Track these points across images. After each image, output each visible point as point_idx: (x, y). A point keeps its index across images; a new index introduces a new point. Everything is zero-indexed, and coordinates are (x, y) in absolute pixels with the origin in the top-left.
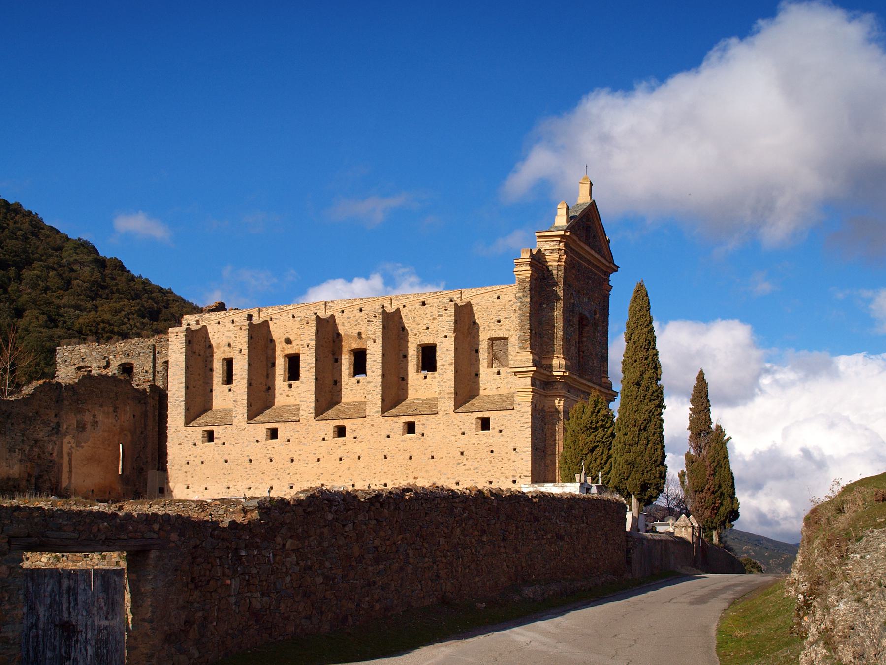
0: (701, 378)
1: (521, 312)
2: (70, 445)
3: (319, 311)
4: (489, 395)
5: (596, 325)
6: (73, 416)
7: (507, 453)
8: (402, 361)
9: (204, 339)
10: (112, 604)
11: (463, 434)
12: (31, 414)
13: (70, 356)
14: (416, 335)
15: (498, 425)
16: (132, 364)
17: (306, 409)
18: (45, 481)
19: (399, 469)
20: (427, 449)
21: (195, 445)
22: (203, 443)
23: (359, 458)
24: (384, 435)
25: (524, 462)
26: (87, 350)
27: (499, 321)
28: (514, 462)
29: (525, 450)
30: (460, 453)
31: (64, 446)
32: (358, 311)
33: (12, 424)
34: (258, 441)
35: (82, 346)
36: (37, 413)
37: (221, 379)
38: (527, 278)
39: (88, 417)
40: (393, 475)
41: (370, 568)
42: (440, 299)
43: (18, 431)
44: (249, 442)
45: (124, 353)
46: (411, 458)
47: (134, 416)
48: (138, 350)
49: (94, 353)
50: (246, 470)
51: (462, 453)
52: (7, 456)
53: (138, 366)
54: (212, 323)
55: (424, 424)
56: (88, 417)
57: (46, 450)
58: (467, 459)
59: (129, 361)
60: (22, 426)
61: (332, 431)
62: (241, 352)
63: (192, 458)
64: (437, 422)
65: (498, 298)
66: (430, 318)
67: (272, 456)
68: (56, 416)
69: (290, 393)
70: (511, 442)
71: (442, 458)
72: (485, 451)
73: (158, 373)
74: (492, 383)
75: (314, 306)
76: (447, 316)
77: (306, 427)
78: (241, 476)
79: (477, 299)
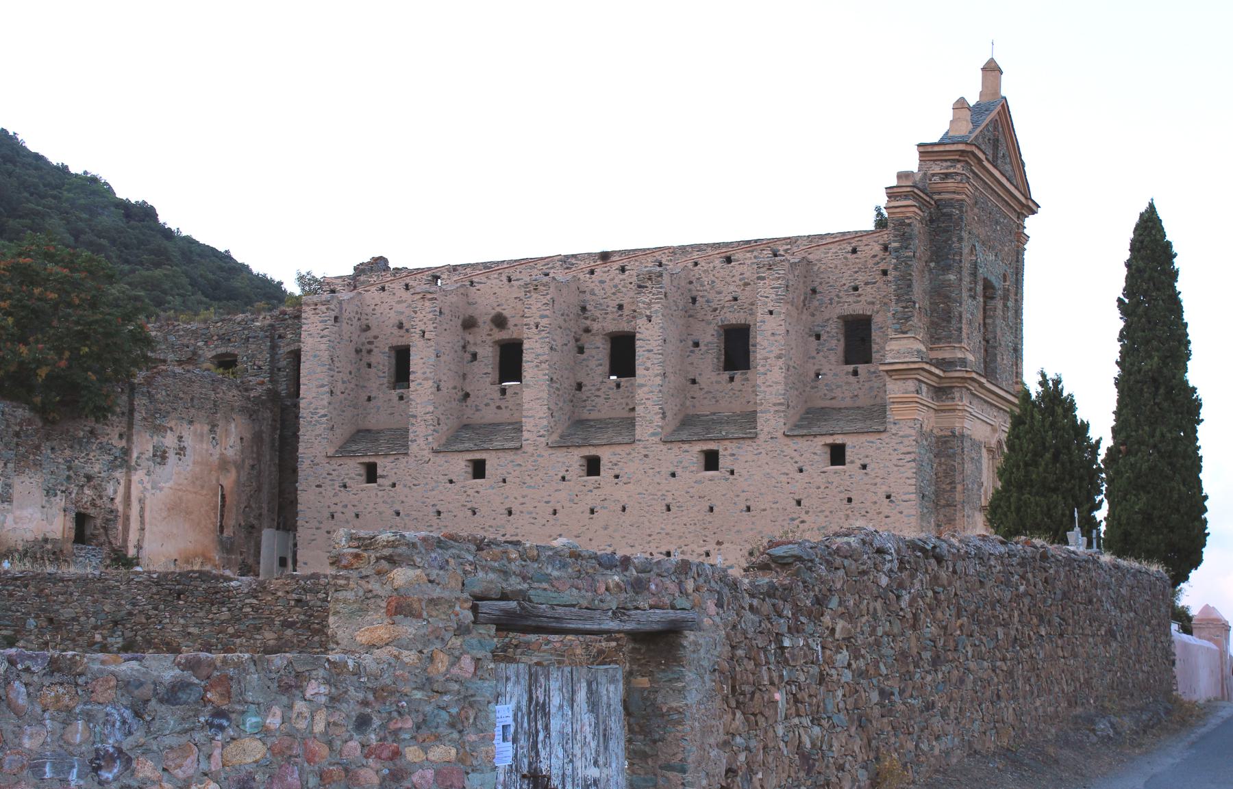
1: (898, 273)
3: (552, 271)
4: (840, 409)
5: (1005, 298)
6: (149, 438)
7: (875, 503)
8: (692, 352)
10: (605, 735)
11: (801, 471)
12: (82, 433)
14: (715, 310)
15: (861, 457)
16: (236, 356)
17: (533, 429)
19: (693, 527)
20: (738, 496)
21: (345, 486)
23: (624, 509)
24: (665, 472)
26: (159, 334)
27: (856, 289)
28: (887, 517)
29: (906, 497)
32: (403, 290)
34: (451, 482)
37: (385, 380)
39: (170, 440)
40: (680, 537)
41: (929, 678)
42: (755, 253)
43: (60, 460)
44: (436, 482)
45: (221, 338)
46: (711, 509)
47: (241, 439)
48: (246, 332)
51: (799, 503)
52: (44, 502)
53: (245, 358)
54: (373, 289)
55: (733, 455)
57: (104, 493)
58: (807, 512)
59: (229, 350)
60: (68, 452)
61: (576, 466)
62: (423, 336)
63: (339, 508)
64: (756, 452)
66: (738, 283)
67: (475, 506)
68: (121, 436)
70: (882, 484)
71: (764, 510)
72: (838, 499)
73: (279, 370)
74: (844, 388)
75: (543, 262)
76: (773, 280)
77: (532, 459)
79: (819, 252)
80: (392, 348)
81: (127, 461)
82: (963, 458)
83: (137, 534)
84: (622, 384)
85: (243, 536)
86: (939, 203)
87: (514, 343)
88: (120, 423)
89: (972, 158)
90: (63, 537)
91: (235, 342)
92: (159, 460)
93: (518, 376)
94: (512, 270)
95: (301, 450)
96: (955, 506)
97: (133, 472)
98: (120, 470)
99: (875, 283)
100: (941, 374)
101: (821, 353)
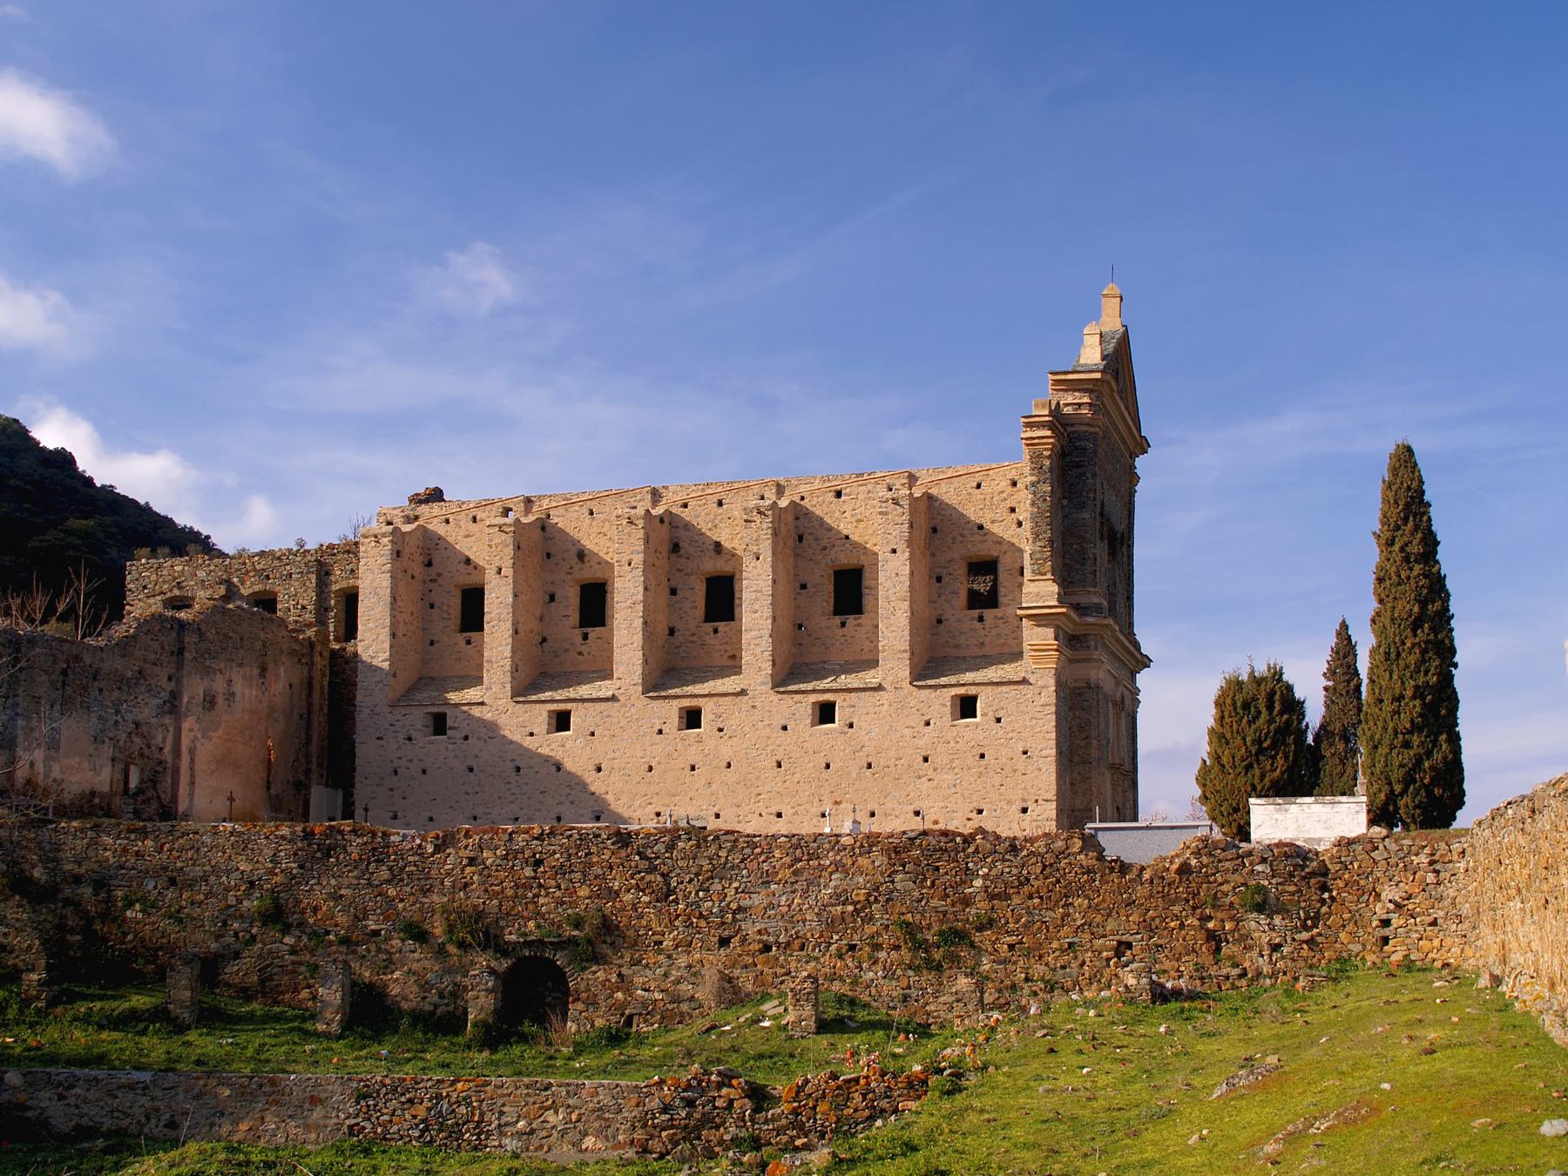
2: (192, 734)
13: (154, 577)
14: (825, 549)
18: (149, 799)
21: (410, 739)
22: (425, 736)
23: (729, 766)
25: (1043, 776)
29: (1044, 753)
30: (921, 758)
31: (183, 736)
32: (715, 505)
33: (101, 690)
35: (178, 560)
36: (140, 673)
38: (1046, 449)
39: (219, 685)
43: (109, 703)
46: (828, 766)
48: (288, 568)
49: (201, 574)
50: (508, 786)
51: (926, 759)
56: (219, 685)
57: (153, 742)
58: (935, 770)
60: (116, 694)
62: (500, 573)
63: (403, 762)
65: (979, 486)
68: (170, 678)
69: (585, 649)
74: (968, 635)
78: (500, 798)
80: (734, 573)
81: (176, 707)
83: (188, 788)
84: (720, 629)
86: (1071, 436)
87: (721, 577)
88: (169, 663)
90: (111, 790)
91: (275, 578)
92: (207, 705)
93: (479, 627)
94: (594, 503)
95: (359, 698)
97: (183, 718)
98: (169, 716)
99: (1002, 521)
100: (1077, 619)
101: (944, 597)
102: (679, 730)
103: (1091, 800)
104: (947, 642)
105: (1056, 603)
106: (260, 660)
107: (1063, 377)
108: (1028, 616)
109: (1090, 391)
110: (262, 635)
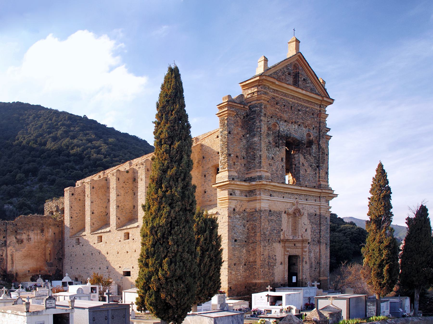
0: (381, 166)
9: (83, 192)
38: (226, 116)
39: (24, 237)
56: (24, 237)
63: (72, 253)
68: (4, 237)
74: (214, 196)
82: (261, 221)
85: (57, 261)
86: (250, 107)
89: (266, 82)
96: (256, 243)
101: (206, 183)
102: (124, 240)
103: (256, 258)
104: (207, 200)
105: (227, 180)
106: (41, 228)
107: (244, 84)
108: (218, 187)
109: (257, 86)
110: (41, 222)
